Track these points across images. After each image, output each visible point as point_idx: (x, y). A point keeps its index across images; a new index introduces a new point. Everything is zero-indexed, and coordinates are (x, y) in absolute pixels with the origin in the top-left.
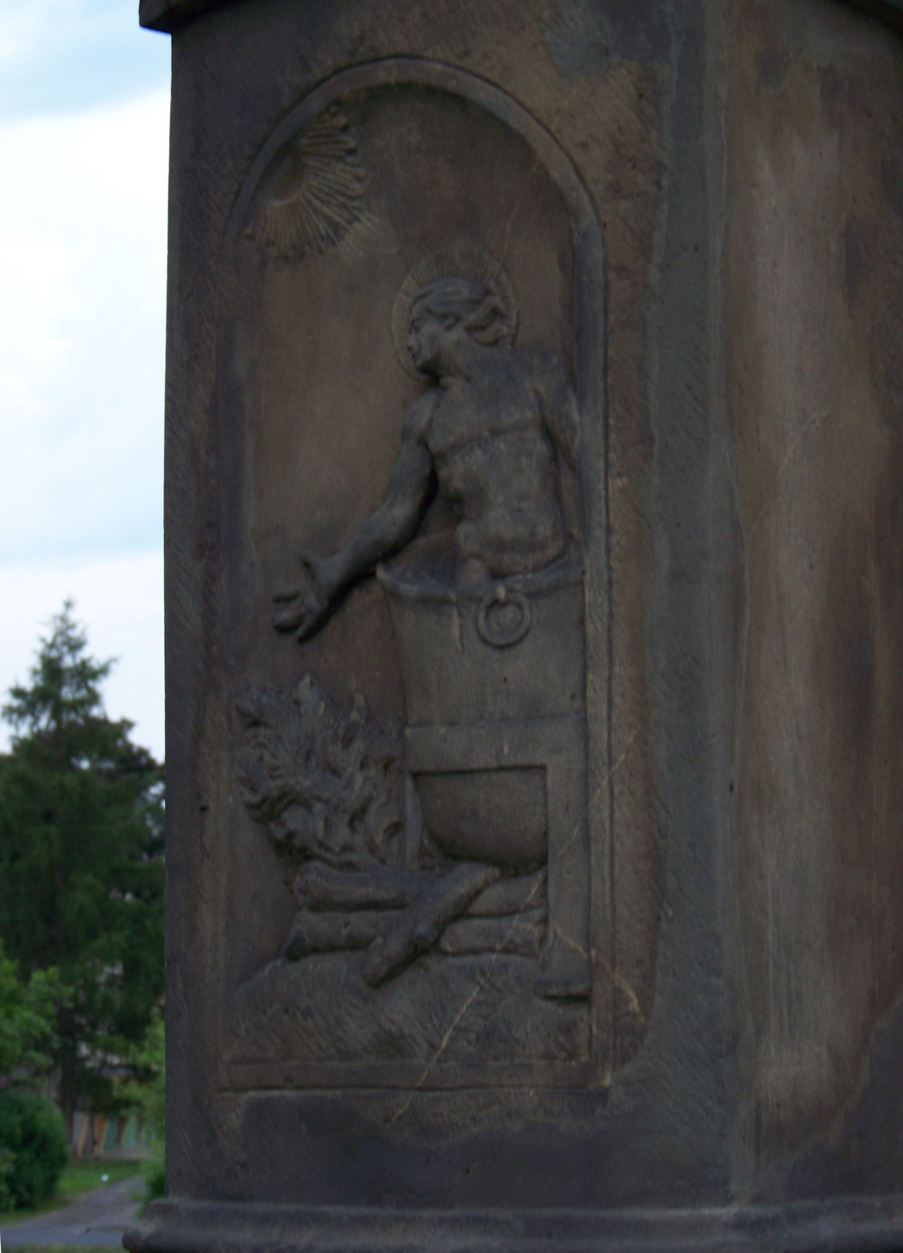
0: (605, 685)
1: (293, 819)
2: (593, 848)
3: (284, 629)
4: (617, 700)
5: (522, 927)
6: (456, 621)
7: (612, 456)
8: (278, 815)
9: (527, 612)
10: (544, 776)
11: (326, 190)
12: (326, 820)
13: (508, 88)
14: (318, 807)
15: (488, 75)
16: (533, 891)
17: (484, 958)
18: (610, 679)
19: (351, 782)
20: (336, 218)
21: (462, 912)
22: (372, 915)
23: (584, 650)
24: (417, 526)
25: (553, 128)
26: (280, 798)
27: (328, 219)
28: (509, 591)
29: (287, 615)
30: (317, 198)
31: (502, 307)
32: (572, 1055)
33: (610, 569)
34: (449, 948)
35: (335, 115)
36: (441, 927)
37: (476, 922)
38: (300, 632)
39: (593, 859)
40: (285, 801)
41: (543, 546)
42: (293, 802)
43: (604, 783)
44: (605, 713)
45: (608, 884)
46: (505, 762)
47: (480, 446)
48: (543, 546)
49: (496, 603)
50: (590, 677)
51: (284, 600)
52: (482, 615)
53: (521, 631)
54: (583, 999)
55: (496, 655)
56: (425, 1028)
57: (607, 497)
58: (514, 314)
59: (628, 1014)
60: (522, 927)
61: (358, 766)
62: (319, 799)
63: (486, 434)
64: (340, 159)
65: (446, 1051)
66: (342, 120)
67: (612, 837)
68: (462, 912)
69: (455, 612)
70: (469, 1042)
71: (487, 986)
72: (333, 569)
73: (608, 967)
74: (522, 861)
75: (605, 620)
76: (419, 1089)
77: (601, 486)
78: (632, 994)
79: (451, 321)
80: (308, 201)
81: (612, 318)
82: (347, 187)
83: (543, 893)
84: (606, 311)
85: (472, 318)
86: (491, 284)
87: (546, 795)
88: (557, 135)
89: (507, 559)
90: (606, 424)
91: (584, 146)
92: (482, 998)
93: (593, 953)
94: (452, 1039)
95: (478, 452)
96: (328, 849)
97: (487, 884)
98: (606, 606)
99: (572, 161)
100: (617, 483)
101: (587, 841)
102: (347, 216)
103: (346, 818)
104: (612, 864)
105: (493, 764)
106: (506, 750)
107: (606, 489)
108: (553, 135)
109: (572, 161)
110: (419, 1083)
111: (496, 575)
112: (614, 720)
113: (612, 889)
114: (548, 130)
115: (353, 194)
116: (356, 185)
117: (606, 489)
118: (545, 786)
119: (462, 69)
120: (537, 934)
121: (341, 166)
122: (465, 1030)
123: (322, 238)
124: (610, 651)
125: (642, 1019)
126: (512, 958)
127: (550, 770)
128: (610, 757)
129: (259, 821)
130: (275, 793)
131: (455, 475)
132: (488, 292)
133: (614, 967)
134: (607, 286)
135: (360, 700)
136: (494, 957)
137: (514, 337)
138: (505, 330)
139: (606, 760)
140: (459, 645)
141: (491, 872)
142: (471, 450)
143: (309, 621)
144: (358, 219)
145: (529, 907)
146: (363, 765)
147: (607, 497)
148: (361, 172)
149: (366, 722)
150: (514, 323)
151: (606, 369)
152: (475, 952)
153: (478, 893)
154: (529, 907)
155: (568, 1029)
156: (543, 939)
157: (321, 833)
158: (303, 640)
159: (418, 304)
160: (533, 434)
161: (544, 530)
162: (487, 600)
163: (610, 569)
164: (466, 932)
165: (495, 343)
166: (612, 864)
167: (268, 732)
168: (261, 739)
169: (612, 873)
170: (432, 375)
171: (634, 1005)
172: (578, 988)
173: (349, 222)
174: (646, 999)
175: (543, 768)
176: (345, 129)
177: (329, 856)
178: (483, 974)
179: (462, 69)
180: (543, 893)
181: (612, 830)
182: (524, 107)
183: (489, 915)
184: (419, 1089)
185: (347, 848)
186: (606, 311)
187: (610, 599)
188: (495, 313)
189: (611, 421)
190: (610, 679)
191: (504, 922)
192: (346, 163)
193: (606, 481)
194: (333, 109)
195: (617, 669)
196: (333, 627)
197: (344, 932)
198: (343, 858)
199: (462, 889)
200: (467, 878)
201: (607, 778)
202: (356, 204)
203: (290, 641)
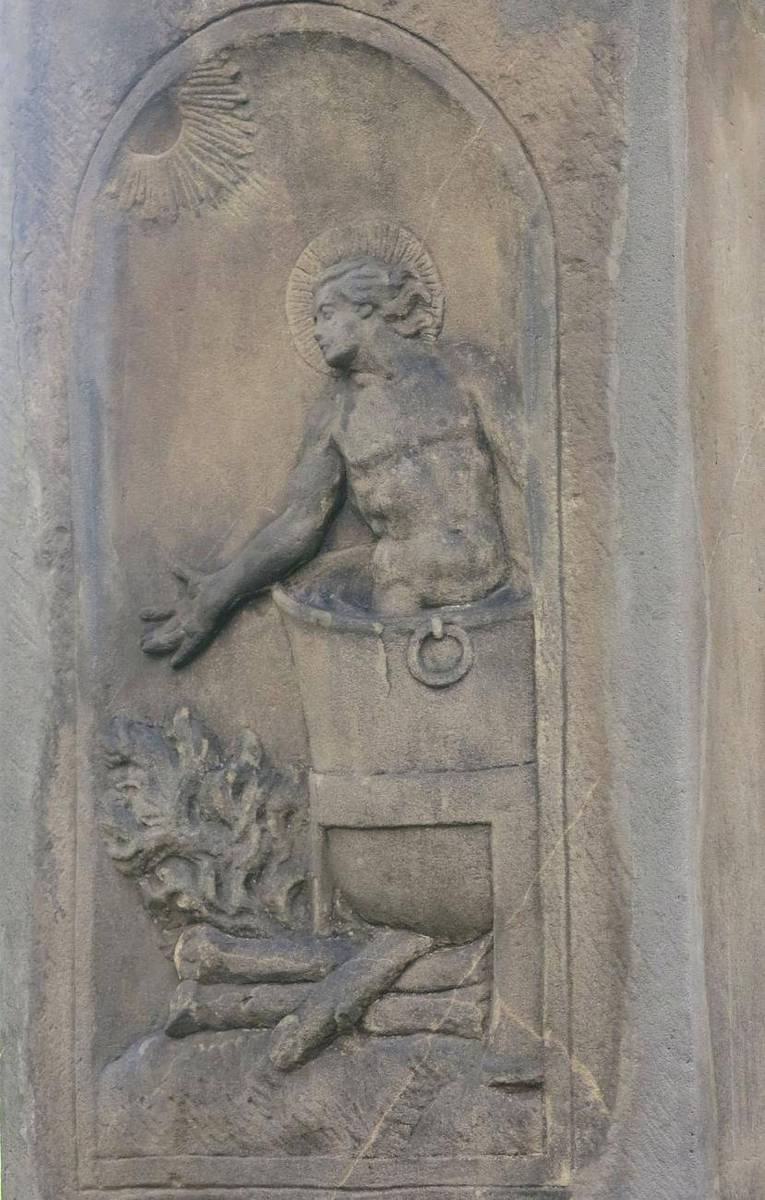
0: (559, 733)
1: (171, 878)
2: (546, 916)
3: (157, 653)
4: (573, 750)
5: (460, 1005)
6: (382, 654)
7: (566, 474)
8: (153, 870)
9: (467, 648)
10: (489, 834)
11: (208, 145)
12: (217, 877)
13: (443, 46)
14: (205, 863)
15: (418, 30)
16: (475, 964)
17: (418, 1040)
18: (564, 728)
19: (244, 835)
20: (219, 178)
21: (389, 987)
22: (277, 989)
23: (534, 693)
24: (322, 540)
25: (495, 96)
26: (160, 848)
27: (208, 178)
28: (446, 624)
29: (161, 637)
30: (197, 152)
31: (425, 294)
32: (523, 1151)
33: (562, 599)
34: (374, 1028)
35: (226, 61)
36: (365, 1005)
37: (405, 998)
38: (175, 658)
39: (546, 929)
40: (163, 855)
41: (484, 573)
42: (175, 855)
43: (560, 843)
44: (559, 765)
45: (564, 957)
46: (445, 819)
47: (409, 456)
48: (484, 573)
49: (429, 638)
50: (542, 724)
51: (156, 620)
52: (414, 649)
53: (462, 671)
54: (535, 1087)
55: (432, 696)
56: (349, 1119)
57: (560, 520)
58: (439, 304)
59: (588, 1104)
60: (460, 1005)
61: (254, 816)
62: (207, 853)
63: (415, 442)
64: (227, 111)
65: (375, 1145)
66: (233, 68)
67: (568, 905)
68: (389, 987)
69: (381, 645)
70: (402, 1136)
71: (423, 1072)
72: (215, 589)
73: (566, 1052)
74: (459, 928)
75: (559, 658)
76: (342, 1188)
77: (554, 507)
78: (592, 1082)
79: (368, 309)
80: (186, 157)
81: (565, 317)
82: (234, 144)
83: (487, 970)
84: (558, 309)
85: (389, 306)
86: (411, 266)
87: (490, 856)
88: (500, 103)
89: (443, 587)
90: (559, 437)
91: (532, 117)
92: (417, 1085)
93: (547, 1035)
94: (384, 1132)
95: (407, 464)
96: (221, 912)
97: (419, 956)
98: (559, 643)
99: (519, 135)
100: (571, 505)
101: (537, 908)
102: (232, 177)
103: (242, 875)
104: (568, 934)
105: (428, 819)
106: (445, 804)
107: (559, 511)
108: (495, 103)
109: (519, 135)
110: (341, 1184)
111: (427, 605)
112: (569, 772)
113: (569, 963)
114: (490, 98)
115: (241, 151)
116: (245, 142)
117: (559, 511)
118: (489, 848)
119: (387, 21)
120: (479, 1014)
121: (228, 119)
122: (398, 1122)
123: (202, 200)
124: (564, 697)
125: (604, 1110)
126: (450, 1039)
127: (494, 824)
128: (565, 815)
129: (128, 875)
130: (153, 845)
131: (374, 490)
132: (408, 276)
133: (571, 1051)
134: (558, 280)
135: (250, 738)
136: (430, 1037)
137: (439, 327)
138: (429, 321)
139: (561, 819)
140: (385, 682)
141: (426, 941)
142: (398, 461)
143: (187, 645)
144: (243, 179)
145: (469, 983)
146: (261, 815)
147: (560, 520)
148: (251, 127)
149: (261, 764)
150: (438, 311)
151: (558, 374)
152: (405, 1032)
153: (409, 964)
154: (469, 983)
155: (521, 1121)
156: (486, 1019)
157: (211, 894)
158: (179, 667)
159: (327, 287)
160: (469, 443)
161: (484, 554)
162: (420, 634)
163: (562, 599)
164: (392, 1010)
165: (417, 335)
166: (568, 934)
167: (140, 772)
168: (130, 782)
169: (569, 944)
170: (344, 367)
171: (595, 1094)
172: (529, 1076)
173: (235, 183)
174: (609, 1087)
175: (488, 825)
176: (236, 78)
177: (222, 920)
178: (419, 1058)
179: (387, 21)
180: (487, 970)
181: (568, 898)
182: (463, 71)
183: (423, 991)
184: (342, 1188)
185: (242, 911)
186: (558, 309)
187: (564, 636)
188: (416, 301)
189: (564, 434)
190: (564, 728)
191: (441, 999)
192: (234, 116)
193: (559, 504)
194: (224, 56)
195: (572, 715)
196: (216, 656)
197: (244, 1008)
198: (238, 922)
199: (391, 961)
200: (386, 951)
201: (562, 839)
202: (242, 162)
203: (165, 664)
